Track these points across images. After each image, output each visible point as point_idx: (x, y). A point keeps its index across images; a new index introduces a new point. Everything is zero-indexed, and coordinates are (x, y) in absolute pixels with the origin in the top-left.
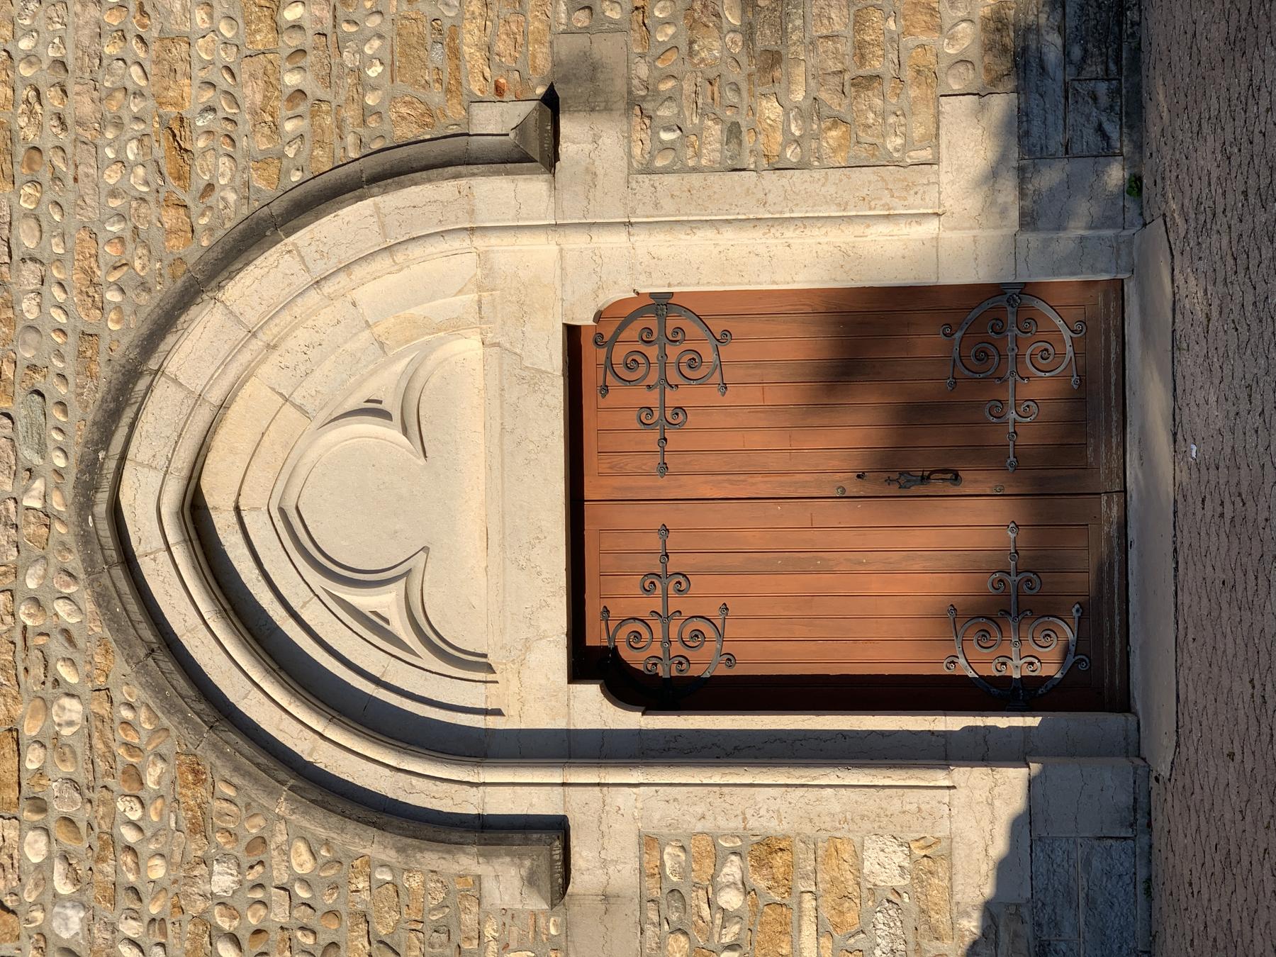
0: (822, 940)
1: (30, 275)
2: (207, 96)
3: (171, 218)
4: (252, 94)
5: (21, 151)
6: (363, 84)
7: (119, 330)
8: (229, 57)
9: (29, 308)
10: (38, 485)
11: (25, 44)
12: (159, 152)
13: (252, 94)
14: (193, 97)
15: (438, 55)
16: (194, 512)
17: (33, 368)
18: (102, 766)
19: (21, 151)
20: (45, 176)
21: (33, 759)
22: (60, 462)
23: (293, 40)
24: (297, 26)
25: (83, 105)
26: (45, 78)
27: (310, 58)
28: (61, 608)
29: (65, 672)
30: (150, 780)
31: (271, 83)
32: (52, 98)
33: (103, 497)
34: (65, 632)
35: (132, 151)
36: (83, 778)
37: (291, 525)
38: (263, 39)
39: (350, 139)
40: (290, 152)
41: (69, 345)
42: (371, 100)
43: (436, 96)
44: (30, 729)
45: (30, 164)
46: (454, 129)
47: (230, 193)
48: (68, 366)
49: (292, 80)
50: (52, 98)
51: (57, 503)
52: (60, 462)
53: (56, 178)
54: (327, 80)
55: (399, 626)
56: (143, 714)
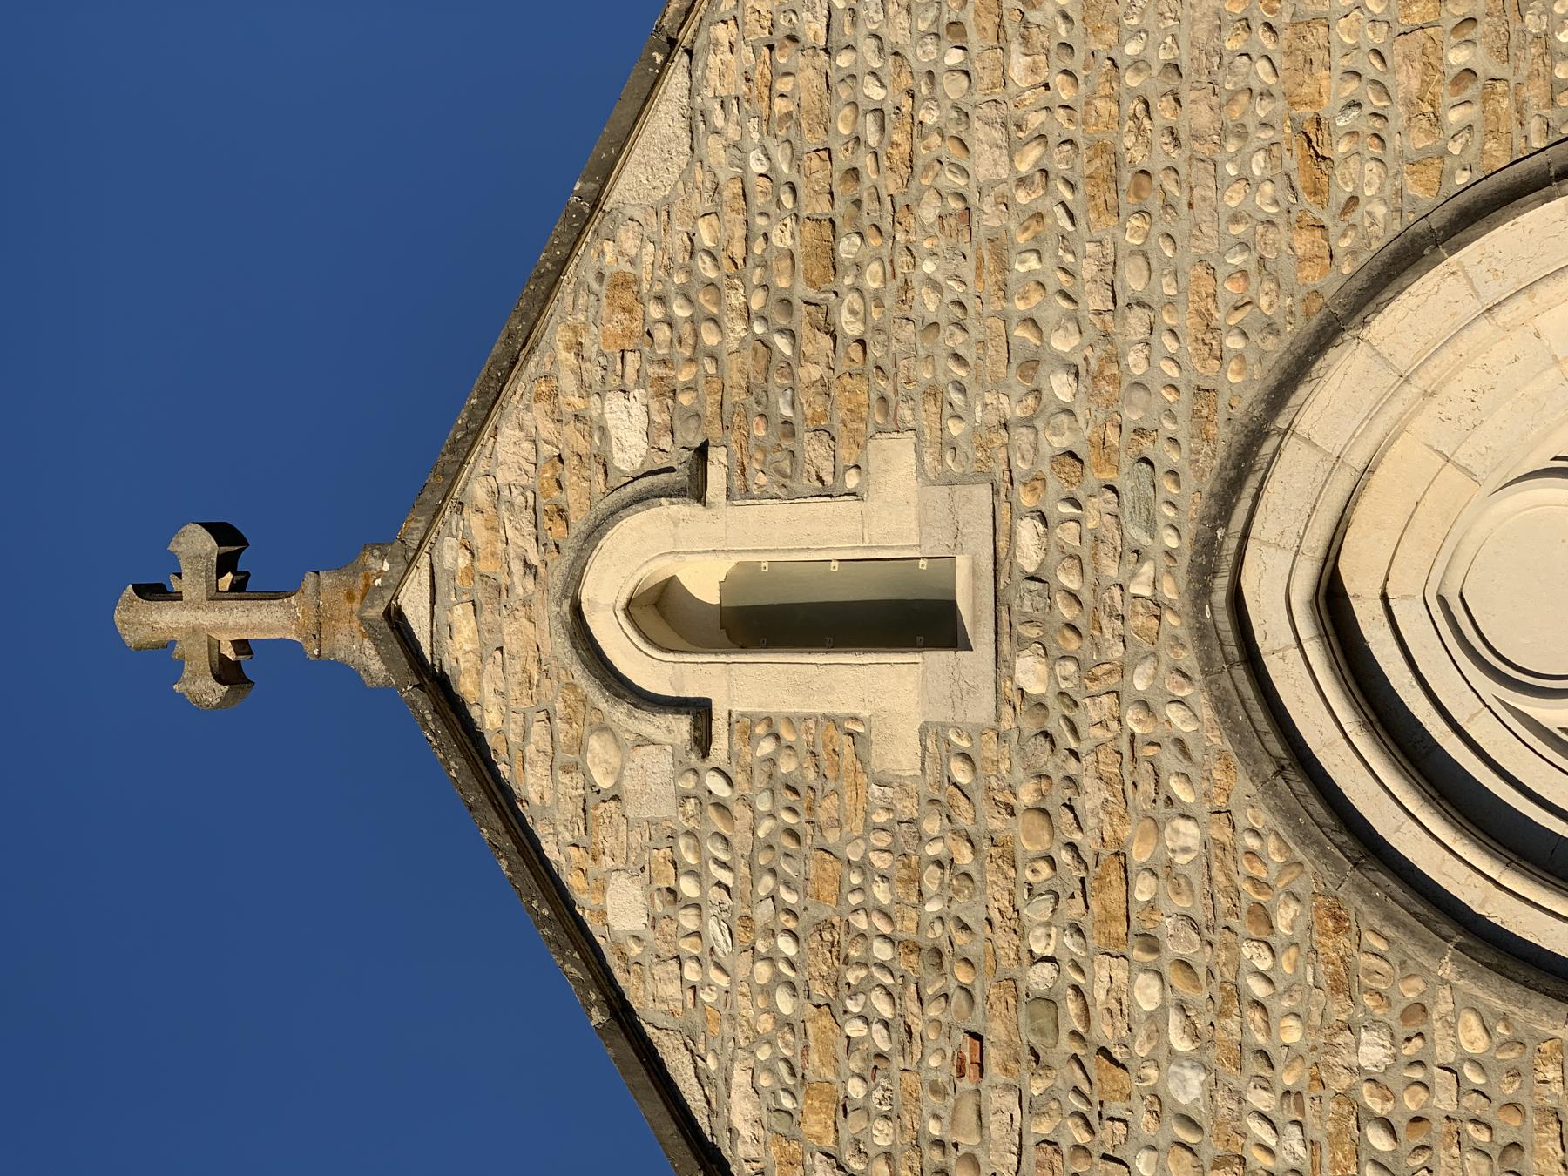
1: (1136, 322)
2: (1351, 88)
3: (1305, 242)
4: (1406, 80)
5: (1127, 177)
7: (1241, 384)
8: (1378, 38)
9: (1136, 361)
10: (1147, 569)
11: (1132, 48)
12: (1291, 163)
13: (1406, 80)
14: (1333, 90)
16: (1332, 602)
17: (1140, 432)
18: (1223, 903)
19: (1127, 177)
20: (1155, 204)
21: (1144, 890)
22: (1172, 542)
25: (1199, 115)
28: (1174, 713)
29: (1178, 789)
33: (1222, 582)
34: (1179, 741)
35: (1258, 166)
36: (1200, 916)
37: (1453, 616)
39: (1534, 125)
40: (1455, 148)
44: (1140, 854)
45: (1137, 190)
49: (1458, 57)
52: (1172, 542)
53: (1168, 205)
54: (1505, 53)
56: (1272, 843)
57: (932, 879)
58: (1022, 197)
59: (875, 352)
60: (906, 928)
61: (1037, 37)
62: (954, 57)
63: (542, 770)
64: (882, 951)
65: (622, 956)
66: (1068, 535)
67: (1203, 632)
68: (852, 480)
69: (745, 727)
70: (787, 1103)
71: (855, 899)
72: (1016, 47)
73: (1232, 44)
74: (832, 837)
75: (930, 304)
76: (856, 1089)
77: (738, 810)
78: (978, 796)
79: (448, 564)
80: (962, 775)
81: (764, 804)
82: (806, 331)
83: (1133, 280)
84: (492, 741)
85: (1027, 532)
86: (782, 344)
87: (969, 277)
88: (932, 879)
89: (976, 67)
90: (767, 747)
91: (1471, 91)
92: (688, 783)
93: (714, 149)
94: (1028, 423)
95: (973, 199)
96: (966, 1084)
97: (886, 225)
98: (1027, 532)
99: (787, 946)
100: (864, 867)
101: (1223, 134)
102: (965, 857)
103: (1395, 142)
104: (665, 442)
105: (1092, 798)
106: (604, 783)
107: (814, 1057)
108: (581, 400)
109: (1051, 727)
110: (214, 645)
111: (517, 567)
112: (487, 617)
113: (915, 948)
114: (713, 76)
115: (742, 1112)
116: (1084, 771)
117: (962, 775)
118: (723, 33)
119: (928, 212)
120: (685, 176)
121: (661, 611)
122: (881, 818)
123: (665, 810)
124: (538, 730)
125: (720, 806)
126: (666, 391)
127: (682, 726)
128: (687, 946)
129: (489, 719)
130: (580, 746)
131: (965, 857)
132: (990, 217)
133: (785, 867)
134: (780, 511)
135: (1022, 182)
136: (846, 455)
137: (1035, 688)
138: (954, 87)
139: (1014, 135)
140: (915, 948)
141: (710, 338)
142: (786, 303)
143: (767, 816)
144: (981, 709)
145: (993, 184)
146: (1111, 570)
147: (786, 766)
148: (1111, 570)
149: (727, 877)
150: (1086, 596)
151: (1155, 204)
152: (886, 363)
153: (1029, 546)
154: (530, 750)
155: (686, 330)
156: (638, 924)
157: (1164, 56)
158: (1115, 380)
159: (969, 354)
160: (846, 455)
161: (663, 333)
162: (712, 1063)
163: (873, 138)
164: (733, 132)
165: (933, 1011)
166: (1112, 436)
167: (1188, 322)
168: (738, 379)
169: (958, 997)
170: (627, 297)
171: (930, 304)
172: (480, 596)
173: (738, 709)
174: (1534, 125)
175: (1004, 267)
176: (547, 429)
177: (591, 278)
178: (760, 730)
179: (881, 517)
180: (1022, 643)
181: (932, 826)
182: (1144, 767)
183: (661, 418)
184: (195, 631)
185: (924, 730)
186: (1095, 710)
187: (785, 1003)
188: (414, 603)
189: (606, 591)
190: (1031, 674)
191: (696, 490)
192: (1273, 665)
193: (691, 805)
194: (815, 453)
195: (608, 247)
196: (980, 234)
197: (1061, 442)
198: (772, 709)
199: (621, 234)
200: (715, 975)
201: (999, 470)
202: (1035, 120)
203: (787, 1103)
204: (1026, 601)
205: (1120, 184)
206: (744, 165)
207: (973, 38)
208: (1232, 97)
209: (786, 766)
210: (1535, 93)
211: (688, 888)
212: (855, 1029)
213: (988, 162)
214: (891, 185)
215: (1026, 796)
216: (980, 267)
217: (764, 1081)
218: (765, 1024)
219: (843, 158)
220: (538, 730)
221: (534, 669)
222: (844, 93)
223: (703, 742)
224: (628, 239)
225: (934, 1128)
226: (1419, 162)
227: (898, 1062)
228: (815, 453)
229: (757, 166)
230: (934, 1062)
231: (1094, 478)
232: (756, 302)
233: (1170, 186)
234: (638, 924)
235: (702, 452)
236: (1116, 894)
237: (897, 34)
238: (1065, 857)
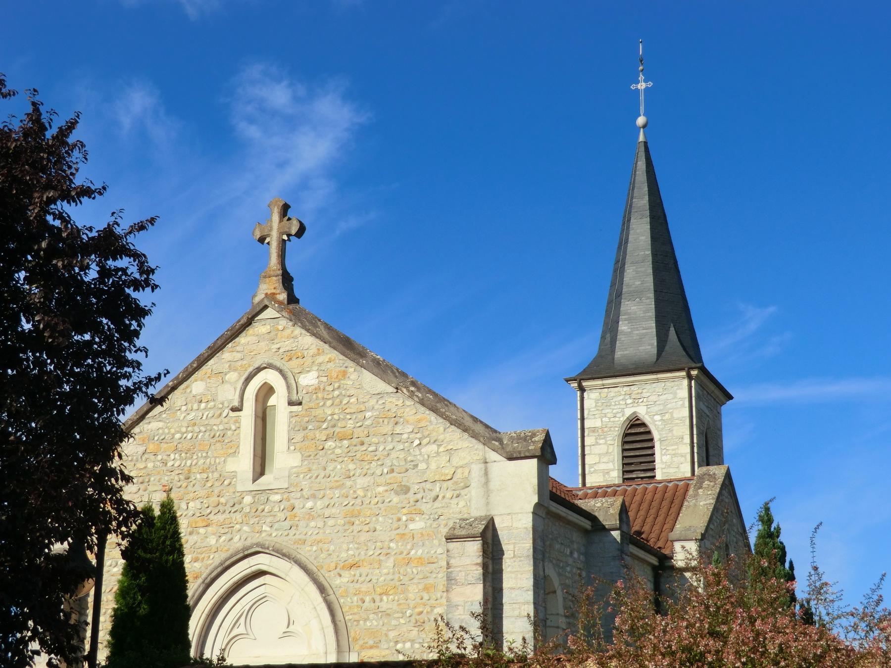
0: (724, 492)
1: (320, 524)
2: (364, 574)
4: (364, 587)
5: (353, 519)
6: (365, 620)
7: (306, 553)
8: (374, 581)
9: (313, 524)
10: (268, 529)
11: (381, 519)
12: (350, 561)
13: (364, 587)
14: (364, 570)
15: (371, 643)
16: (261, 573)
17: (297, 526)
18: (199, 551)
19: (353, 519)
20: (347, 527)
21: (202, 531)
22: (274, 535)
23: (377, 598)
24: (381, 600)
25: (364, 537)
26: (371, 526)
27: (373, 604)
28: (238, 537)
29: (223, 538)
30: (196, 564)
31: (367, 593)
32: (366, 528)
33: (260, 550)
34: (232, 539)
35: (351, 552)
36: (197, 546)
37: (262, 599)
38: (379, 590)
39: (351, 617)
40: (349, 599)
41: (303, 537)
42: (361, 622)
43: (361, 642)
44: (209, 529)
45: (349, 523)
46: (352, 647)
47: (338, 582)
48: (297, 537)
49: (367, 599)
50: (366, 528)
51: (264, 534)
52: (274, 535)
53: (345, 531)
55: (235, 632)
56: (211, 562)
57: (205, 475)
58: (351, 492)
59: (321, 453)
60: (194, 470)
61: (386, 494)
62: (385, 471)
63: (230, 358)
64: (189, 463)
65: (187, 387)
66: (276, 509)
67: (251, 547)
68: (292, 448)
69: (237, 421)
70: (156, 438)
71: (200, 455)
72: (386, 488)
73: (379, 544)
74: (213, 447)
75: (330, 466)
76: (159, 457)
77: (219, 420)
78: (221, 488)
79: (281, 322)
80: (226, 483)
81: (221, 427)
82: (327, 432)
83: (331, 522)
84: (237, 340)
85: (277, 497)
86: (324, 426)
87: (336, 479)
88: (205, 475)
89: (382, 478)
90: (233, 428)
91: (360, 603)
92: (226, 404)
93: (373, 402)
94: (302, 496)
95: (353, 479)
96: (161, 487)
97: (350, 454)
98: (277, 497)
99: (189, 436)
100: (206, 457)
101: (359, 544)
102: (209, 484)
103: (352, 585)
104: (304, 392)
105: (221, 517)
106: (227, 377)
107: (166, 446)
108: (315, 363)
109: (236, 505)
110: (268, 235)
111: (278, 346)
112: (267, 336)
113: (189, 471)
114: (390, 400)
115: (155, 425)
116: (226, 515)
117: (226, 483)
118: (400, 403)
119: (351, 466)
120: (368, 393)
121: (267, 391)
122: (217, 460)
123: (220, 398)
124: (239, 356)
125: (220, 415)
126: (317, 390)
127: (236, 404)
128: (189, 406)
129: (242, 339)
130: (235, 370)
131: (209, 484)
132: (349, 483)
133: (208, 434)
134: (286, 428)
135: (355, 492)
136: (298, 446)
137: (245, 500)
138: (379, 472)
139: (366, 489)
140: (189, 471)
141: (329, 403)
142: (334, 426)
143: (218, 429)
144: (240, 488)
145: (355, 484)
146: (269, 520)
147: (229, 433)
148: (269, 520)
149: (204, 418)
150: (264, 513)
151: (347, 527)
152: (318, 456)
153: (276, 498)
154: (235, 354)
155: (330, 396)
156: (194, 392)
157: (378, 528)
158: (309, 519)
159: (318, 480)
160: (298, 446)
161: (331, 388)
162: (164, 416)
163: (371, 449)
164: (376, 407)
165: (176, 478)
166: (297, 519)
167: (319, 537)
168: (317, 413)
169: (179, 484)
170: (340, 377)
171: (330, 466)
172: (272, 334)
173: (242, 419)
174: (351, 617)
175: (337, 488)
176: (311, 352)
177: (346, 365)
178: (237, 425)
179: (283, 458)
180: (254, 497)
181: (216, 475)
182: (227, 530)
183: (310, 389)
184: (271, 229)
185: (235, 472)
186: (238, 516)
187: (178, 436)
188: (269, 313)
189: (270, 377)
190: (248, 499)
191: (291, 403)
192: (246, 561)
193: (221, 406)
194: (299, 437)
195: (352, 370)
196: (344, 481)
197: (296, 505)
198: (242, 429)
199: (356, 373)
200: (183, 415)
201: (291, 489)
202: (369, 494)
203: (156, 438)
204: (263, 498)
205: (351, 517)
206: (369, 411)
207: (390, 476)
208: (366, 545)
209: (229, 433)
210: (356, 617)
211: (203, 405)
212: (172, 456)
213: (361, 482)
214: (359, 455)
215: (223, 500)
216: (337, 481)
217: (161, 431)
218: (173, 431)
219: (366, 440)
220: (239, 356)
221: (255, 353)
222: (382, 439)
223: (234, 410)
224: (354, 376)
225: (152, 479)
226: (346, 591)
227: (165, 469)
228: (299, 437)
229: (368, 414)
230: (166, 478)
231: (288, 514)
232: (336, 417)
233: (350, 531)
234: (194, 392)
235: (300, 404)
236: (201, 524)
237: (394, 455)
238: (209, 511)
